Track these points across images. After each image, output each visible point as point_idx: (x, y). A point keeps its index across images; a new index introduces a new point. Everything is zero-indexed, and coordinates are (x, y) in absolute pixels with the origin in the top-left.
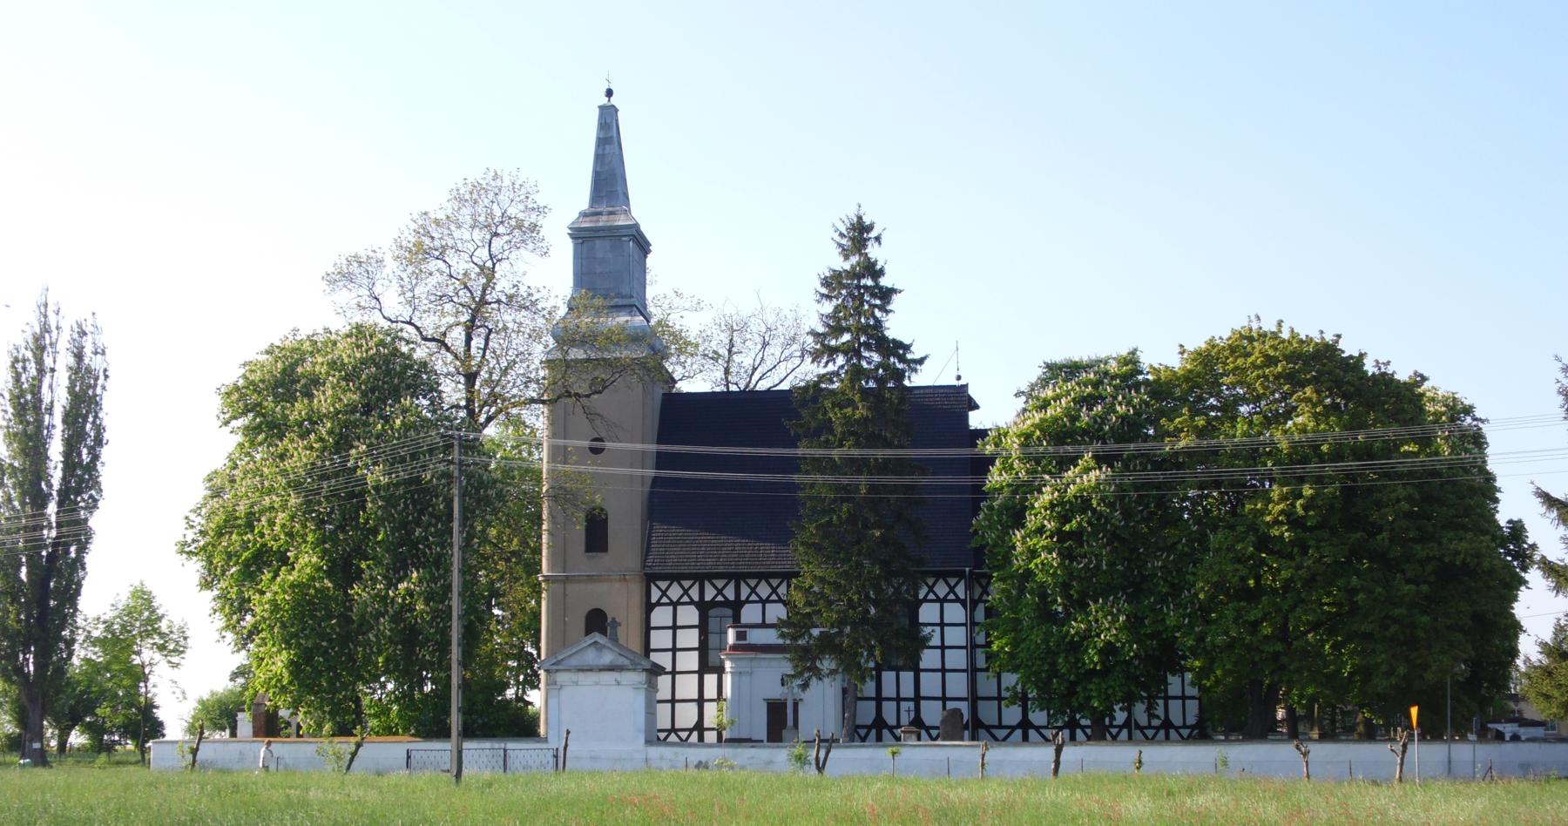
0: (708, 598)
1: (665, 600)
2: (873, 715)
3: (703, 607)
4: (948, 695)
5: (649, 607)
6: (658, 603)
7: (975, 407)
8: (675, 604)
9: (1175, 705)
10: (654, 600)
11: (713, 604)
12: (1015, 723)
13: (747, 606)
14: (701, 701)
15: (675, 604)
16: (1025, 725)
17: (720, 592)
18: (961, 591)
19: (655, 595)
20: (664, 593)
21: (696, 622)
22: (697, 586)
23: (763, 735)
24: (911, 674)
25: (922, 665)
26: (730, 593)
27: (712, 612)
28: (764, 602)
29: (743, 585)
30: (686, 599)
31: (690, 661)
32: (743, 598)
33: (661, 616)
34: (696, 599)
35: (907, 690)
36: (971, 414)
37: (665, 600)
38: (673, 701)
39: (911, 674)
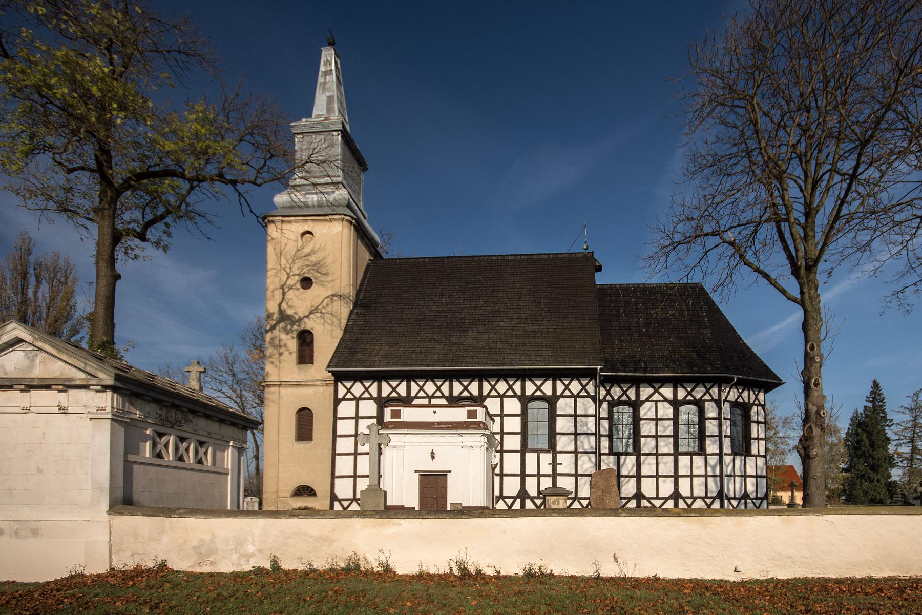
0: (456, 393)
1: (349, 396)
2: (518, 488)
3: (525, 400)
4: (353, 451)
5: (337, 402)
6: (344, 399)
7: (599, 269)
8: (502, 397)
9: (699, 469)
10: (340, 396)
11: (533, 398)
12: (667, 495)
13: (343, 403)
14: (523, 475)
15: (357, 400)
16: (792, 505)
17: (394, 389)
18: (591, 388)
19: (342, 391)
20: (349, 391)
21: (519, 430)
22: (447, 384)
23: (413, 502)
24: (550, 455)
25: (558, 449)
26: (547, 388)
27: (530, 405)
28: (575, 397)
29: (413, 384)
30: (366, 395)
31: (666, 446)
32: (485, 393)
33: (346, 409)
34: (519, 393)
35: (546, 469)
36: (597, 275)
37: (494, 393)
38: (355, 476)
39: (550, 455)
